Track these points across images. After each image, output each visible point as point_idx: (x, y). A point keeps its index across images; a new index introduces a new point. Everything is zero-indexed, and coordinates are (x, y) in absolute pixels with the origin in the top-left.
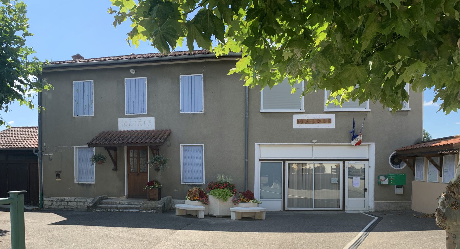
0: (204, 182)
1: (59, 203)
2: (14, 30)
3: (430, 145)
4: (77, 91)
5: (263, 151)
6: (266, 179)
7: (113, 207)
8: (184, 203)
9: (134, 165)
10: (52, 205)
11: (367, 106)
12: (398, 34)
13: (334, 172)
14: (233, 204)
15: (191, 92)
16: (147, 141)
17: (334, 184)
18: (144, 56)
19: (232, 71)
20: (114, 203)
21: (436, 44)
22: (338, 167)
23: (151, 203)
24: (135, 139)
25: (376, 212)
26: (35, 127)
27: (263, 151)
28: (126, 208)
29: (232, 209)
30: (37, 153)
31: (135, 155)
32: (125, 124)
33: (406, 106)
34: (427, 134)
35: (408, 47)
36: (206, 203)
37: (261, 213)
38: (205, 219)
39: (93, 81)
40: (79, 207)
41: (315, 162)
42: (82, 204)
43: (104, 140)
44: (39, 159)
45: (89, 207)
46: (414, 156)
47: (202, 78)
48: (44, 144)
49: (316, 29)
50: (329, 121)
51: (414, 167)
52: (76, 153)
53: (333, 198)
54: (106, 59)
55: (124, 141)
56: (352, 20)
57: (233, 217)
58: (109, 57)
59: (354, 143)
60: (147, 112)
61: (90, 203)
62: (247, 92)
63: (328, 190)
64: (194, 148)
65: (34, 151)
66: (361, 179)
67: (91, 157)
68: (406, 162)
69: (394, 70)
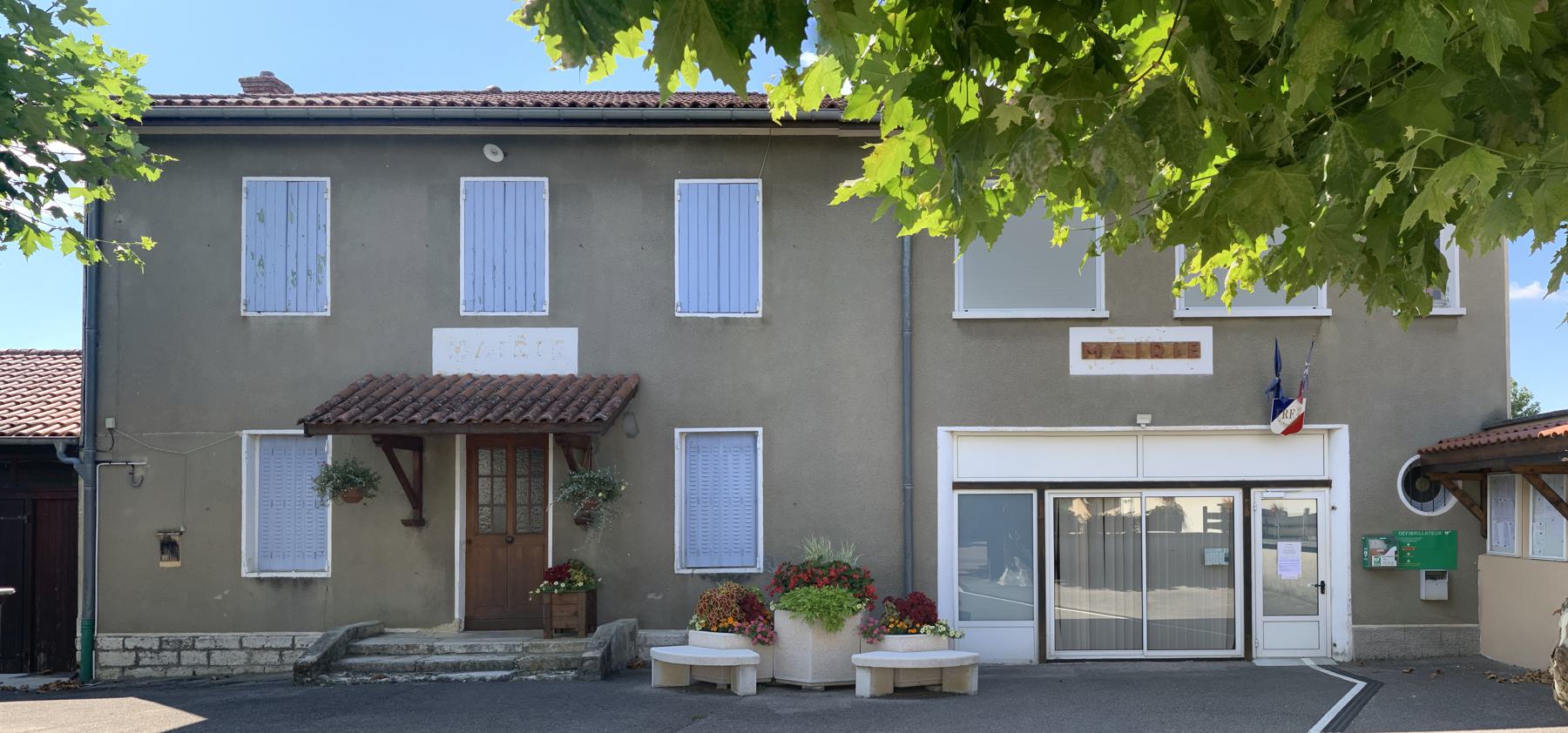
0: (760, 564)
1: (169, 657)
3: (1534, 433)
4: (261, 217)
5: (967, 455)
6: (979, 554)
7: (403, 666)
8: (685, 641)
9: (491, 505)
10: (136, 665)
11: (1317, 302)
12: (1406, 55)
13: (1214, 526)
14: (864, 641)
15: (716, 236)
16: (547, 415)
17: (1214, 566)
18: (539, 98)
19: (845, 191)
20: (408, 650)
21: (1538, 88)
22: (1228, 510)
23: (557, 647)
24: (500, 408)
25: (1359, 665)
26: (66, 354)
27: (967, 455)
28: (456, 667)
29: (858, 658)
30: (77, 456)
31: (500, 468)
32: (458, 350)
33: (1452, 302)
34: (1525, 398)
35: (1444, 101)
36: (765, 637)
37: (961, 669)
38: (759, 698)
39: (328, 179)
40: (258, 669)
41: (1146, 492)
42: (273, 657)
43: (372, 410)
44: (81, 482)
45: (300, 670)
46: (1482, 471)
48: (110, 423)
49: (1135, 34)
50: (1192, 350)
51: (1483, 508)
52: (251, 457)
53: (1213, 615)
54: (386, 99)
55: (453, 415)
56: (1255, 8)
57: (864, 686)
58: (399, 94)
59: (1278, 425)
60: (546, 308)
61: (307, 651)
63: (1194, 590)
64: (726, 441)
65: (60, 448)
66: (1304, 549)
67: (316, 472)
68: (1454, 490)
69: (1394, 177)
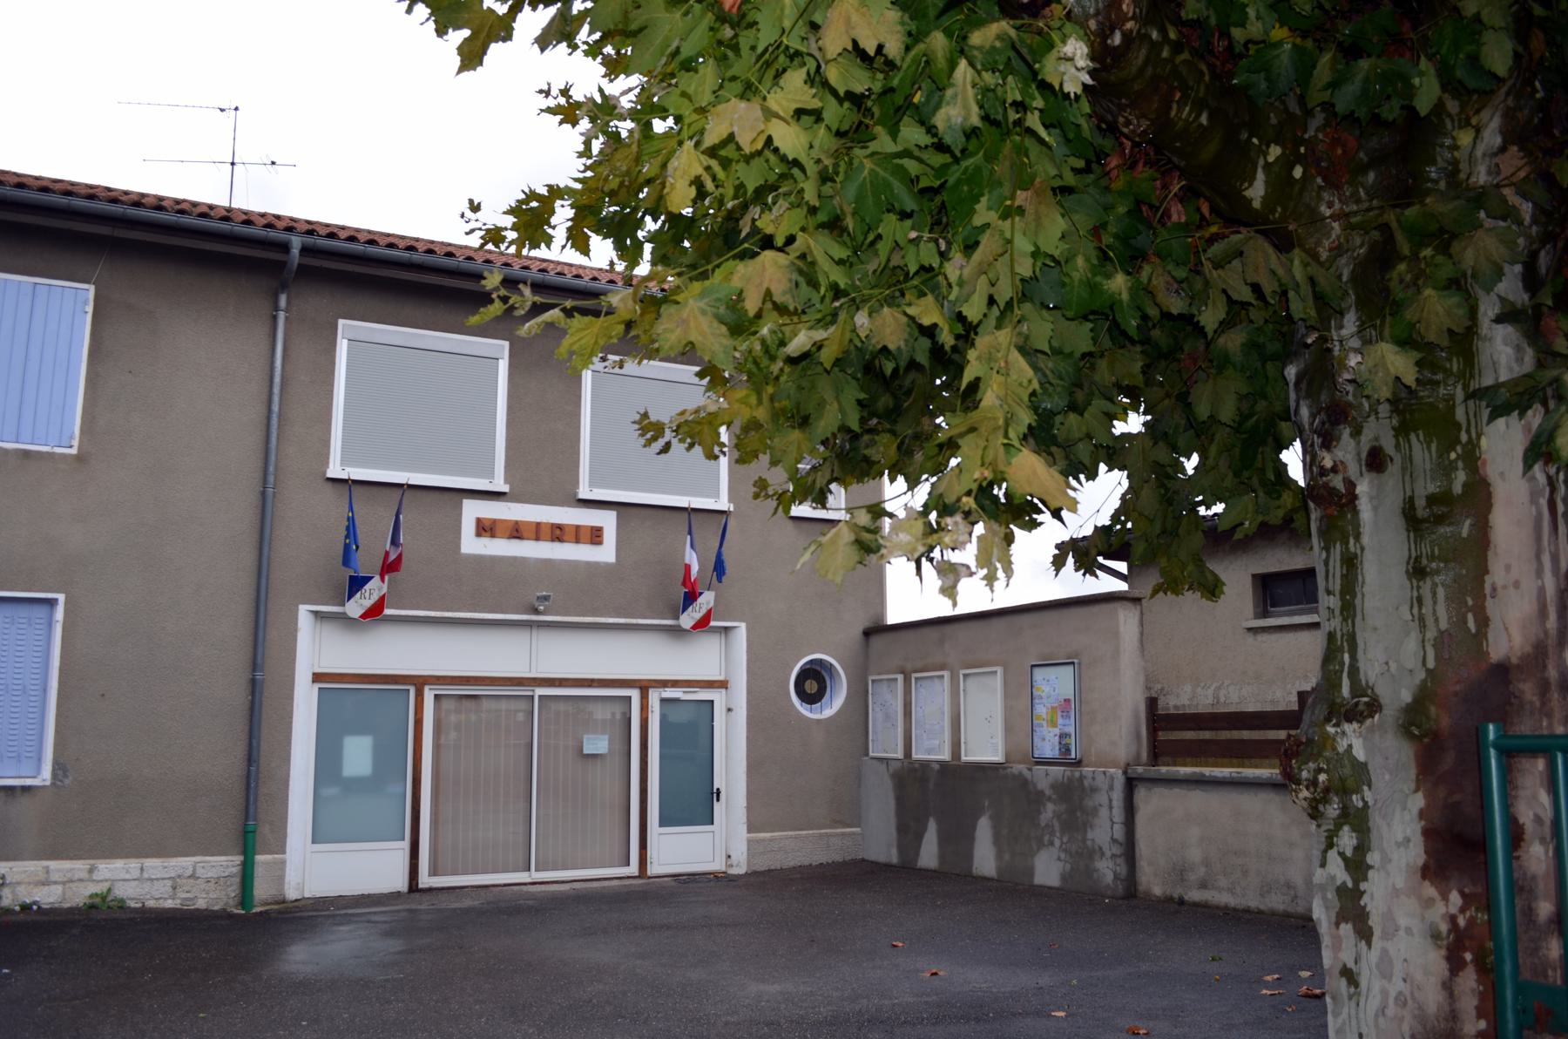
2: (938, 42)
47: (86, 303)
50: (595, 536)
62: (276, 390)
